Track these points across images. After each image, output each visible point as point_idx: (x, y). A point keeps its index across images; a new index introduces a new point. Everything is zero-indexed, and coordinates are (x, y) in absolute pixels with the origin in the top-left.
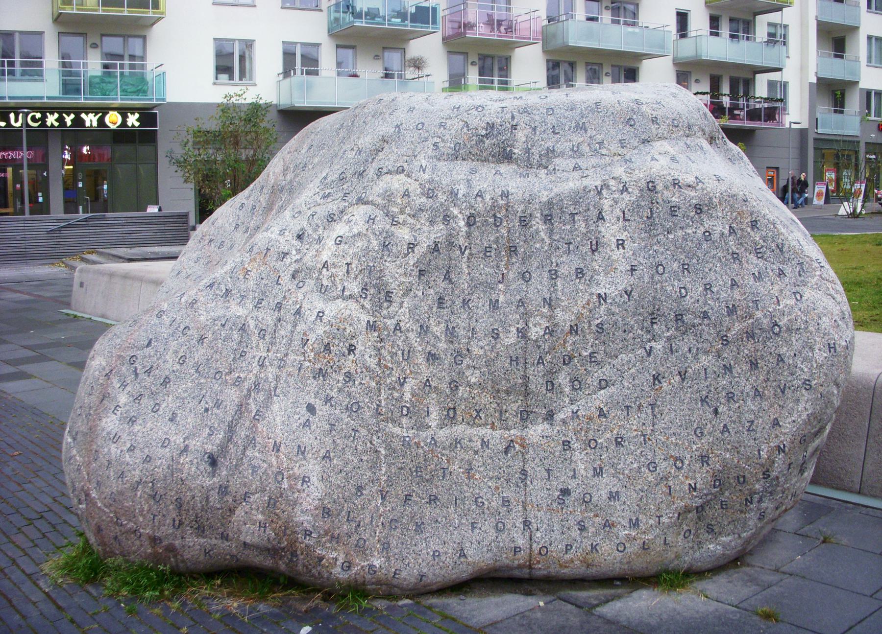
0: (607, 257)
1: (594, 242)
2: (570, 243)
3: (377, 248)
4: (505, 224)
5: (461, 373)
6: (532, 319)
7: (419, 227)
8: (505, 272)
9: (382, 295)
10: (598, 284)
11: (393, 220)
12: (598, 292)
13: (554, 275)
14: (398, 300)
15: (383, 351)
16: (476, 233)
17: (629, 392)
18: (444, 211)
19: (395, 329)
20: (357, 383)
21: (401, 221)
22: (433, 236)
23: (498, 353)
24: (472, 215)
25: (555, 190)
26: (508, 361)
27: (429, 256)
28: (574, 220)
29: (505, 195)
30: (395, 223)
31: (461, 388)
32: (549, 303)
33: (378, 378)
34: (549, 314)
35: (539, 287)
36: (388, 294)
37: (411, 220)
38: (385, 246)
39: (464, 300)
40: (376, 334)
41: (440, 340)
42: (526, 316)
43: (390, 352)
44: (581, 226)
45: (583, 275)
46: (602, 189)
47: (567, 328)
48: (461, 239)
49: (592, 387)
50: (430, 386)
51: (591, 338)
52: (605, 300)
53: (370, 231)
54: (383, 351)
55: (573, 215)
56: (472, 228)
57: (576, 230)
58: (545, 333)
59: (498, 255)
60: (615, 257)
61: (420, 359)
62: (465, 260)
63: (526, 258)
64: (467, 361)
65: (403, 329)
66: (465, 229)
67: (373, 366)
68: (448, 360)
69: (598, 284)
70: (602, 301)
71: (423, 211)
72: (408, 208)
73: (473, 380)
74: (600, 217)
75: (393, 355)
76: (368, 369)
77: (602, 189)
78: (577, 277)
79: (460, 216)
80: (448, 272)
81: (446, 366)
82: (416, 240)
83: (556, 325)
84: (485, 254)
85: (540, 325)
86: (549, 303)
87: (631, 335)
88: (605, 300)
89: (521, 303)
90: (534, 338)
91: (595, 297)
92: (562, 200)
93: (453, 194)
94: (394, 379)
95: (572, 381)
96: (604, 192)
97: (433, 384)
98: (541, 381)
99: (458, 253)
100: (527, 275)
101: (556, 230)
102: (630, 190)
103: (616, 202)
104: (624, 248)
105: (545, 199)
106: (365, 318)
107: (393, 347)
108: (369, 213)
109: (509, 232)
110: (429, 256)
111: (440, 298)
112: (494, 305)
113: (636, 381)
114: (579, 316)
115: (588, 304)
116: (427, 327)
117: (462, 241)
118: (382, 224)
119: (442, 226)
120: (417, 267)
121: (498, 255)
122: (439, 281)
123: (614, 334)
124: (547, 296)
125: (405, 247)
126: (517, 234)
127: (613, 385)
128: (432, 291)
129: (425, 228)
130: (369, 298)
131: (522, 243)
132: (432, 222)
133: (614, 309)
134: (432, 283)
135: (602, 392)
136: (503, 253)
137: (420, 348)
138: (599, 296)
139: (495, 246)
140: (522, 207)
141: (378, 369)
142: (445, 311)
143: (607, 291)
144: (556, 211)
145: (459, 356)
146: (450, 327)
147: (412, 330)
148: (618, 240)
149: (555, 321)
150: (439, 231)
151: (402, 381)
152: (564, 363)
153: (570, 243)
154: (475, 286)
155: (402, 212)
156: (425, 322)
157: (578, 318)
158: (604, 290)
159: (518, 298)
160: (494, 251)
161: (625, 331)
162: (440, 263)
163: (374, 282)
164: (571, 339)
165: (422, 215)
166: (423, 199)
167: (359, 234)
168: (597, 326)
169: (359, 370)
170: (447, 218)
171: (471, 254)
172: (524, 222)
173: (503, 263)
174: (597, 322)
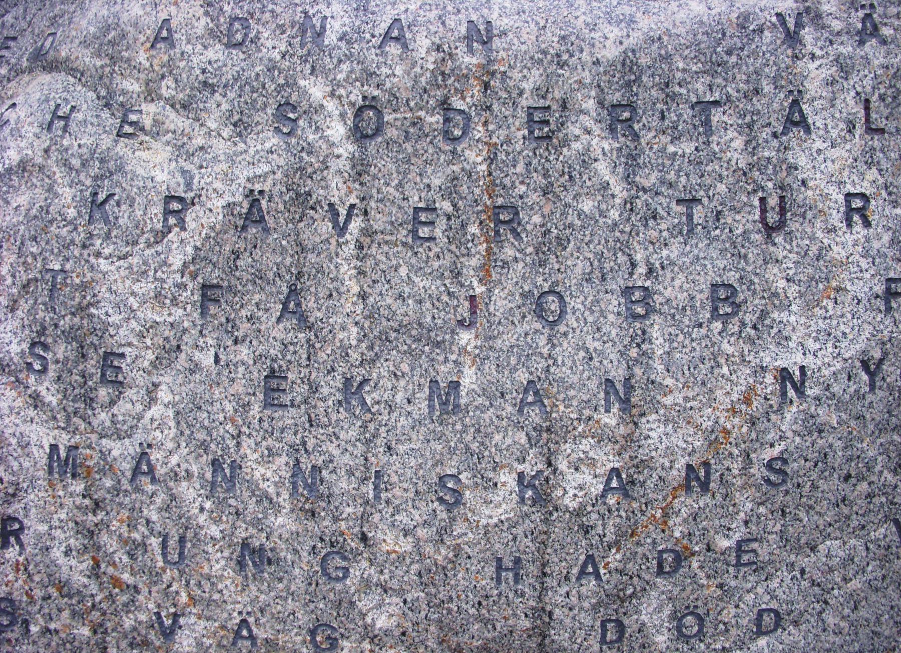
0: (814, 249)
1: (773, 201)
2: (695, 200)
3: (72, 213)
4: (479, 132)
5: (344, 605)
6: (567, 447)
7: (199, 141)
8: (479, 289)
9: (92, 366)
10: (782, 340)
11: (124, 121)
12: (780, 363)
13: (640, 304)
14: (141, 379)
15: (104, 538)
16: (385, 164)
17: (838, 640)
18: (280, 88)
19: (136, 471)
20: (34, 629)
21: (147, 123)
22: (243, 173)
23: (457, 549)
24: (370, 104)
25: (645, 23)
26: (490, 570)
27: (231, 242)
28: (707, 123)
29: (481, 36)
30: (129, 129)
31: (345, 643)
32: (625, 396)
33: (96, 615)
34: (622, 430)
35: (592, 345)
36: (110, 359)
37: (176, 121)
38: (96, 205)
39: (348, 381)
40: (78, 487)
41: (277, 509)
42: (548, 436)
43: (124, 541)
44: (732, 145)
45: (737, 306)
46: (799, 25)
47: (677, 474)
48: (335, 182)
49: (733, 632)
50: (252, 637)
51: (745, 503)
52: (800, 390)
53: (54, 155)
54: (104, 538)
55: (704, 107)
56: (371, 147)
57: (714, 157)
58: (607, 489)
59: (457, 235)
60: (838, 253)
61: (219, 563)
62: (349, 250)
63: (550, 245)
64: (360, 569)
65: (161, 471)
66: (347, 149)
67: (79, 580)
68: (302, 567)
69: (782, 340)
70: (791, 393)
71: (213, 89)
72: (169, 81)
73: (382, 622)
74: (796, 120)
75: (135, 549)
76: (63, 587)
77: (799, 25)
78: (715, 314)
79: (331, 106)
80: (293, 291)
81: (298, 585)
82: (189, 186)
83: (642, 465)
84: (414, 232)
85: (593, 463)
86: (625, 396)
87: (864, 487)
88: (800, 390)
89: (535, 392)
90: (573, 505)
91: (769, 379)
92: (667, 58)
93: (310, 32)
94: (143, 617)
95: (677, 618)
96: (808, 34)
97: (261, 634)
98: (588, 621)
99: (326, 227)
100: (552, 303)
101: (649, 155)
102: (886, 31)
103: (844, 68)
104: (867, 224)
105: (611, 52)
106: (42, 435)
107: (132, 527)
108: (56, 97)
109: (491, 160)
110: (231, 242)
111: (272, 374)
112: (446, 398)
113: (863, 613)
114: (717, 438)
115: (747, 401)
116: (236, 467)
117: (337, 190)
118: (91, 132)
119: (273, 141)
120: (194, 276)
121: (457, 235)
122: (267, 322)
123: (814, 487)
124: (618, 374)
125: (157, 210)
126: (520, 168)
127: (796, 623)
128: (244, 353)
129: (220, 147)
130: (52, 374)
131: (534, 197)
132: (241, 127)
133: (827, 415)
134: (244, 328)
135: (762, 642)
136: (474, 229)
137: (214, 531)
138: (784, 375)
139: (447, 206)
140: (535, 77)
141: (94, 588)
142: (288, 418)
143: (809, 361)
144: (648, 94)
145: (334, 555)
146: (306, 465)
147: (189, 475)
148: (848, 196)
149: (642, 454)
150: (262, 158)
151: (168, 622)
152: (660, 571)
153: (695, 200)
154: (381, 337)
155: (151, 95)
156: (225, 449)
157: (712, 444)
158: (799, 358)
159: (523, 377)
160: (442, 223)
161: (848, 477)
162: (269, 260)
163: (65, 323)
164: (685, 504)
165: (211, 105)
166: (216, 52)
167: (23, 166)
168: (769, 466)
169: (38, 593)
170: (289, 114)
171: (368, 232)
172: (544, 126)
173: (474, 262)
174: (768, 454)
